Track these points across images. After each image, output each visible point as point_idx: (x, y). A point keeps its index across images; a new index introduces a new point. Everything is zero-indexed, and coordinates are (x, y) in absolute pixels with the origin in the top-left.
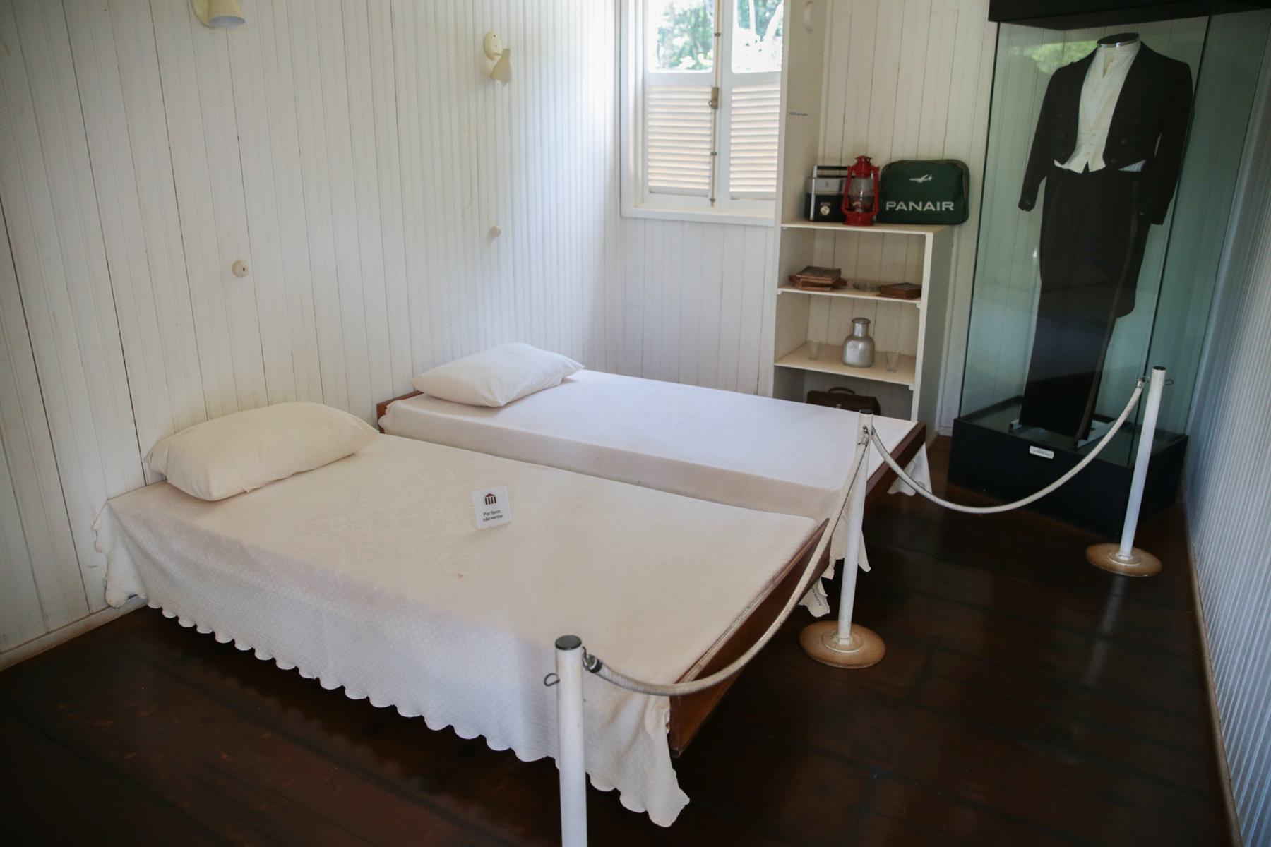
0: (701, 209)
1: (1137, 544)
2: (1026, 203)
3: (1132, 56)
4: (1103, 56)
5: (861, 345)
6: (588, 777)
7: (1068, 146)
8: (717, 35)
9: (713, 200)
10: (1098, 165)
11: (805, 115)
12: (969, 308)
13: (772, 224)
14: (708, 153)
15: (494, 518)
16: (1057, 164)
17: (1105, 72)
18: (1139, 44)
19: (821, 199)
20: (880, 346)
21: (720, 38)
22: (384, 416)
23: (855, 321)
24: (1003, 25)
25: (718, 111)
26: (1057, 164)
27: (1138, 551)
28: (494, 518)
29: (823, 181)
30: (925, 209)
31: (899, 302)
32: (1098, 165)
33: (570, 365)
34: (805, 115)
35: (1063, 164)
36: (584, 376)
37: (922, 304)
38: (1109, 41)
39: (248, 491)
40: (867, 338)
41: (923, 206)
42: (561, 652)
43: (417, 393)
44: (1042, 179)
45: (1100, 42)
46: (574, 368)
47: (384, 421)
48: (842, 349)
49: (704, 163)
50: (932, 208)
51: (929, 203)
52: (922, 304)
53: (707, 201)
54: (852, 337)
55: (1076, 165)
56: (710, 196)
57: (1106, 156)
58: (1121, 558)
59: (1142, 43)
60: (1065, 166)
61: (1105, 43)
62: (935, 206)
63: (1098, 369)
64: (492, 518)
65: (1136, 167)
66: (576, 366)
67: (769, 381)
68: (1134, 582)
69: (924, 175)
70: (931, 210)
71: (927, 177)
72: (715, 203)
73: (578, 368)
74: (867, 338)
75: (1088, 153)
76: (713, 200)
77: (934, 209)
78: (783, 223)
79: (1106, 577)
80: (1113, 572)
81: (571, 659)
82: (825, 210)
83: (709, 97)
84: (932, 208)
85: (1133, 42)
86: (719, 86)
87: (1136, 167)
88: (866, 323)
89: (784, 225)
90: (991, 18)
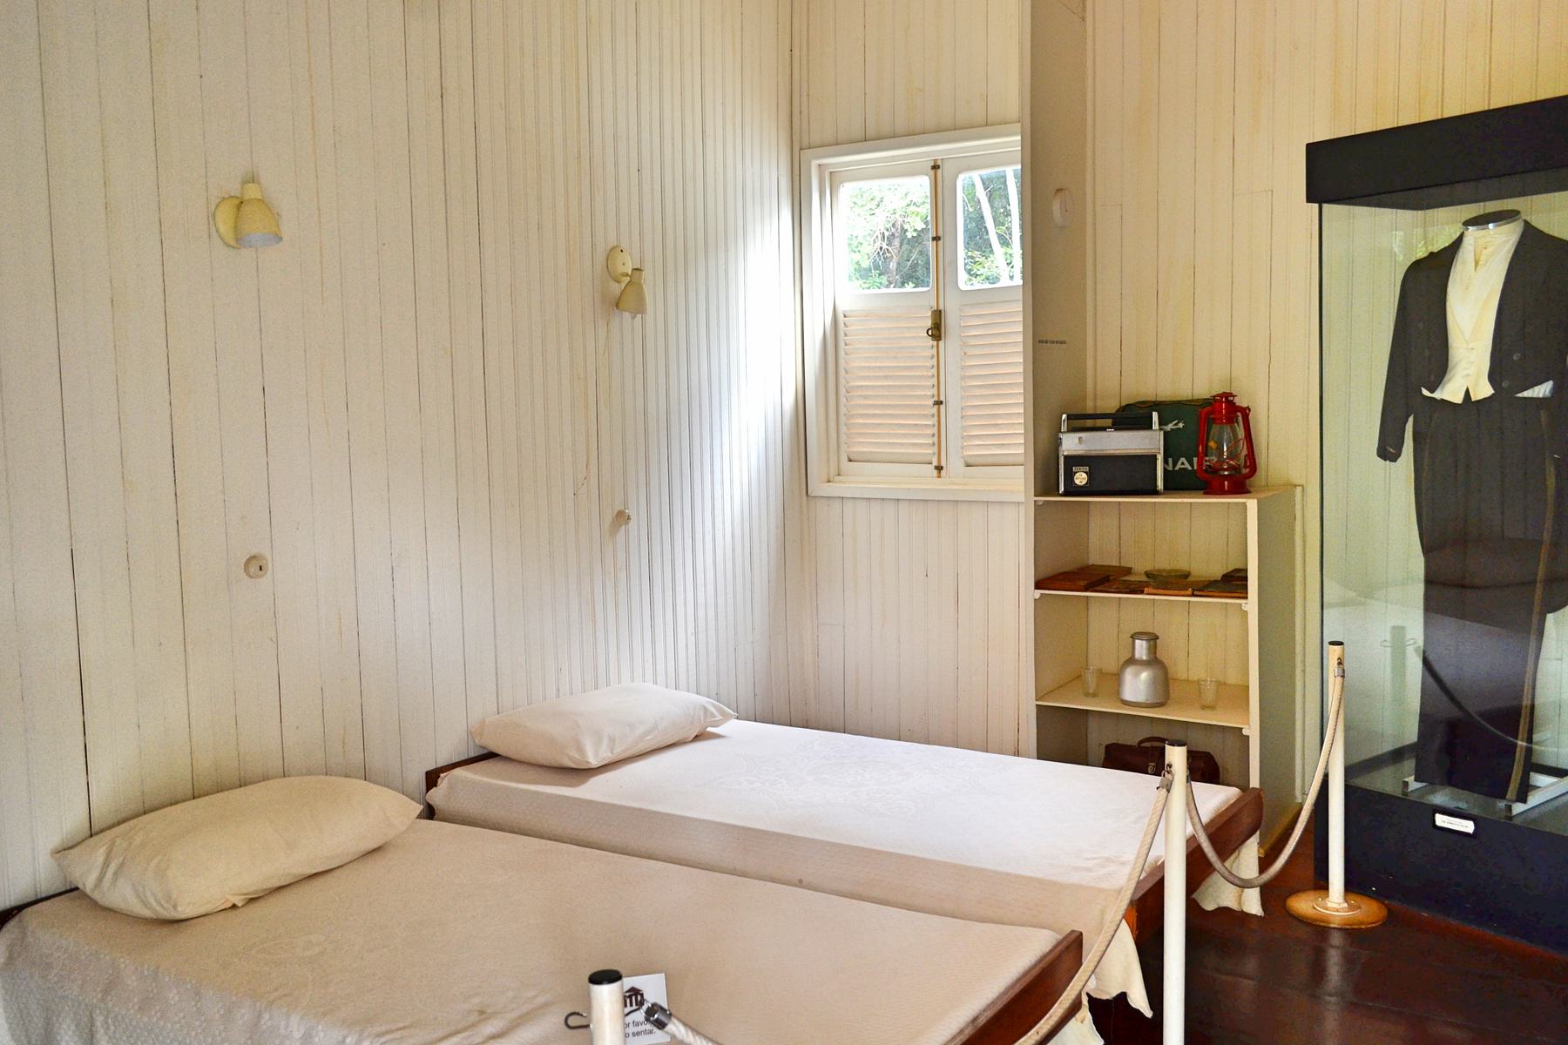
0: (921, 480)
1: (1351, 886)
2: (1388, 450)
3: (1511, 242)
4: (1472, 242)
5: (1145, 675)
6: (729, 737)
7: (1439, 367)
8: (936, 239)
9: (939, 468)
10: (1484, 390)
11: (1061, 342)
12: (1319, 616)
13: (1022, 499)
14: (931, 402)
15: (638, 1034)
16: (1425, 392)
17: (1477, 263)
18: (1523, 224)
19: (1074, 461)
20: (1180, 670)
21: (940, 242)
22: (434, 789)
23: (1134, 637)
24: (1325, 206)
25: (941, 343)
26: (1425, 392)
27: (1352, 896)
28: (638, 1034)
29: (1077, 435)
30: (1177, 468)
31: (1149, 600)
32: (1484, 390)
33: (713, 710)
34: (1061, 342)
35: (1432, 392)
36: (734, 728)
37: (1251, 604)
38: (1480, 221)
39: (240, 905)
40: (1154, 661)
41: (1174, 466)
42: (591, 985)
43: (490, 756)
44: (1409, 416)
45: (1468, 223)
46: (719, 717)
47: (437, 796)
48: (1117, 678)
49: (925, 416)
50: (1187, 466)
51: (1183, 460)
52: (1251, 604)
53: (930, 469)
54: (1131, 661)
55: (1451, 391)
56: (935, 463)
57: (1492, 378)
58: (1329, 905)
59: (1527, 223)
60: (1437, 395)
61: (1473, 225)
62: (1192, 464)
63: (1526, 702)
64: (634, 1034)
65: (1542, 390)
66: (723, 713)
67: (1030, 735)
68: (1353, 934)
69: (1171, 422)
70: (1186, 469)
71: (1176, 424)
72: (943, 472)
73: (726, 717)
74: (1154, 661)
75: (1468, 375)
76: (939, 468)
77: (1190, 468)
78: (1035, 496)
79: (1319, 930)
80: (1325, 924)
81: (607, 997)
82: (1081, 478)
83: (929, 324)
84: (1187, 466)
85: (1513, 221)
86: (941, 307)
87: (1542, 390)
88: (1153, 639)
89: (1037, 498)
90: (1310, 199)
